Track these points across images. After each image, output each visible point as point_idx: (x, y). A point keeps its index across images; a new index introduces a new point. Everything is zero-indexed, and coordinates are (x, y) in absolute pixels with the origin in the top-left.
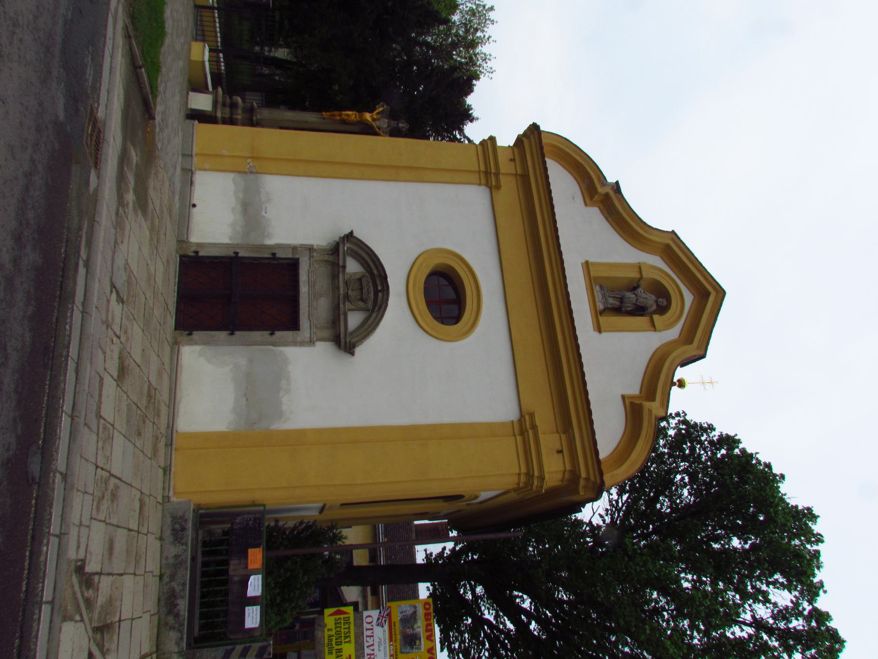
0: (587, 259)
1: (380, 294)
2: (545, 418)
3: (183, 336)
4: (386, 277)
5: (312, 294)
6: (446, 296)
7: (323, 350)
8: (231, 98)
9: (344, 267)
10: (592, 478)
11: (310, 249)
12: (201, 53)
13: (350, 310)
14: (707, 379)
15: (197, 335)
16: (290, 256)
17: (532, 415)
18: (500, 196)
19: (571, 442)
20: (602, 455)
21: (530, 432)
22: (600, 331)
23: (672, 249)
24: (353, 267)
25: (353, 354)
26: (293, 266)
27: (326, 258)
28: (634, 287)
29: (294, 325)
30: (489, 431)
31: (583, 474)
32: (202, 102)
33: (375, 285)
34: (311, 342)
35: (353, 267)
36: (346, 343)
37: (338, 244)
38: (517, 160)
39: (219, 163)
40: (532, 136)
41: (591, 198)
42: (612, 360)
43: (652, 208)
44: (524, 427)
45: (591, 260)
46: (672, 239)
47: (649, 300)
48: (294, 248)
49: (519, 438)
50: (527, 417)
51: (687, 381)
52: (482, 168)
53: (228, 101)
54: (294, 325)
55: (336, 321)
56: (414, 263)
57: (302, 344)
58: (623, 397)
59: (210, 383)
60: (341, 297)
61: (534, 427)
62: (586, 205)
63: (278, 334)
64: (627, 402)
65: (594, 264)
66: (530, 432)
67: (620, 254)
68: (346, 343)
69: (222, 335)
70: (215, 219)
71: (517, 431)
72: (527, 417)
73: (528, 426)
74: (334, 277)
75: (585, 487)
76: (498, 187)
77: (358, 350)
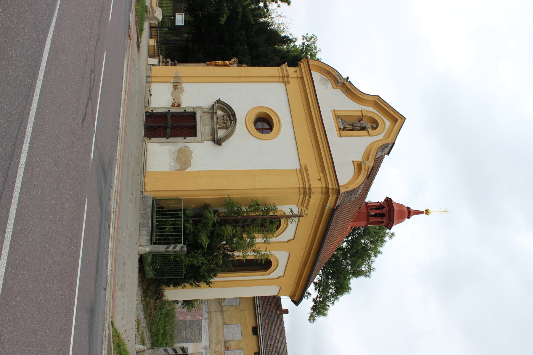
3: (146, 139)
4: (235, 114)
5: (202, 124)
6: (264, 123)
7: (209, 145)
8: (166, 60)
9: (216, 112)
10: (335, 188)
11: (201, 108)
12: (153, 42)
13: (219, 128)
15: (153, 139)
16: (192, 111)
17: (305, 166)
19: (325, 175)
23: (378, 103)
25: (220, 145)
28: (360, 119)
29: (195, 135)
30: (286, 172)
31: (331, 187)
32: (155, 61)
33: (230, 119)
34: (202, 141)
35: (220, 113)
36: (218, 142)
37: (213, 105)
39: (162, 80)
41: (336, 85)
42: (348, 150)
43: (365, 85)
44: (303, 171)
45: (336, 109)
46: (378, 99)
47: (368, 125)
53: (164, 61)
54: (195, 135)
55: (213, 133)
57: (198, 142)
58: (353, 162)
59: (161, 154)
62: (333, 88)
63: (187, 138)
64: (355, 164)
65: (337, 111)
66: (304, 172)
67: (351, 107)
68: (218, 142)
69: (164, 139)
70: (161, 99)
74: (212, 118)
75: (332, 193)
76: (289, 82)
77: (223, 144)
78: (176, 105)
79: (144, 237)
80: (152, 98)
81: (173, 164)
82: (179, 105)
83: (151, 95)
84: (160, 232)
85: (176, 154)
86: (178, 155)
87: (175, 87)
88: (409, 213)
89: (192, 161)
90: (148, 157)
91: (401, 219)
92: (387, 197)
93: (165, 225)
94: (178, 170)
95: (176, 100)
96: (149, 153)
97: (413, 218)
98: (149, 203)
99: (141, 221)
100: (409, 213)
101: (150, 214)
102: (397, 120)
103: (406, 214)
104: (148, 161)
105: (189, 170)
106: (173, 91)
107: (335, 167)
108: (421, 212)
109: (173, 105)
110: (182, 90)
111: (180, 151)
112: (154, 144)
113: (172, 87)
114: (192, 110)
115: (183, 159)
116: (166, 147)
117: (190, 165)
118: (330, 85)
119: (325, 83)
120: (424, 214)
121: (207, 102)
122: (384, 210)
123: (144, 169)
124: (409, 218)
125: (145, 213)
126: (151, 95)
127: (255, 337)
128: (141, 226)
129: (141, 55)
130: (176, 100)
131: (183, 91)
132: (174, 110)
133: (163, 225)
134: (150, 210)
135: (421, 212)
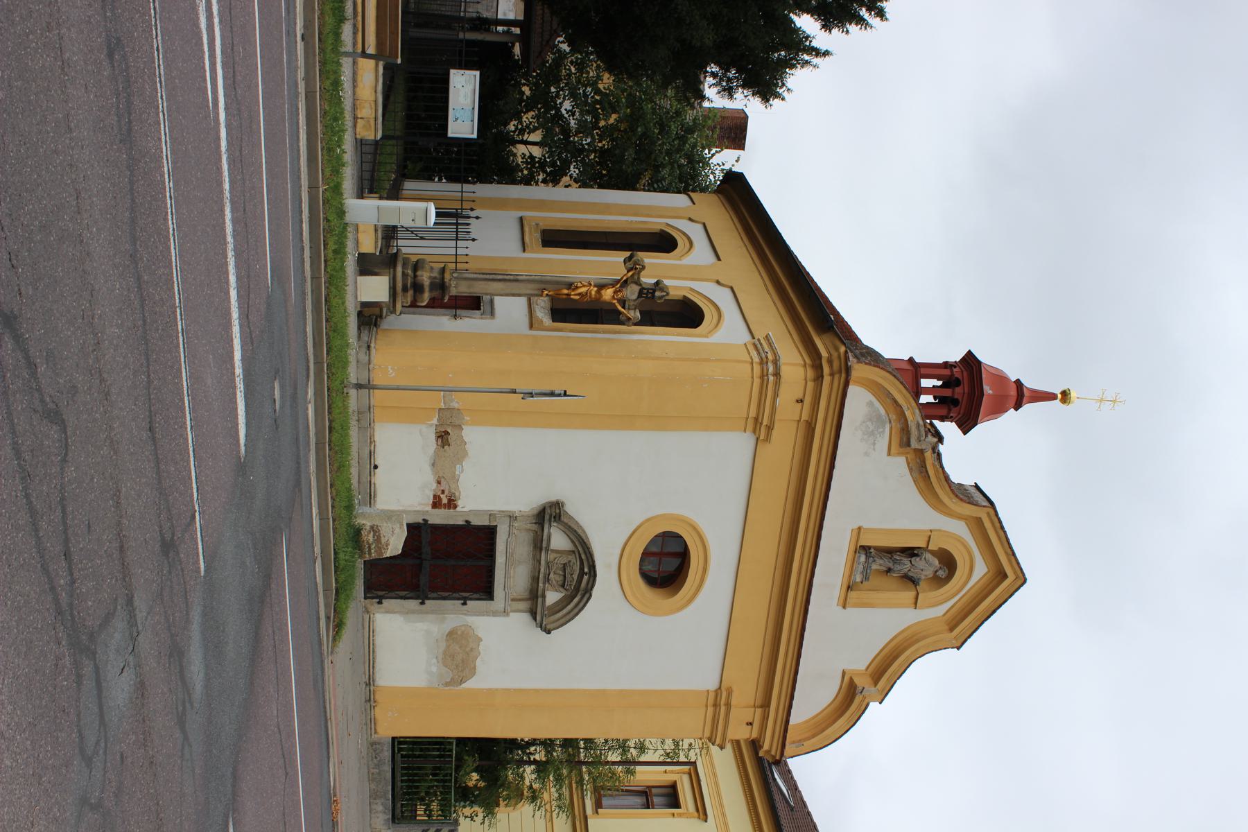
1: (586, 577)
3: (372, 604)
5: (511, 568)
7: (519, 621)
9: (544, 596)
11: (512, 517)
14: (1110, 395)
16: (487, 523)
17: (730, 692)
18: (764, 449)
19: (765, 718)
24: (558, 540)
26: (489, 533)
29: (485, 590)
34: (505, 613)
37: (544, 510)
38: (808, 400)
40: (837, 377)
48: (491, 515)
49: (711, 710)
51: (1073, 394)
52: (753, 414)
54: (485, 590)
55: (534, 597)
56: (634, 532)
59: (404, 643)
66: (723, 708)
69: (413, 604)
71: (711, 701)
72: (724, 694)
73: (723, 702)
78: (445, 501)
80: (380, 478)
81: (434, 669)
82: (452, 504)
83: (376, 467)
84: (409, 781)
85: (443, 645)
86: (448, 647)
87: (443, 437)
88: (1020, 396)
89: (478, 662)
90: (377, 650)
91: (998, 410)
93: (417, 787)
94: (447, 684)
95: (444, 486)
96: (379, 640)
97: (1027, 408)
98: (387, 754)
99: (373, 786)
100: (1020, 396)
101: (389, 775)
103: (1013, 401)
104: (378, 660)
105: (470, 684)
108: (1050, 397)
109: (436, 504)
110: (461, 455)
111: (451, 634)
114: (484, 521)
115: (459, 656)
116: (420, 625)
117: (473, 672)
118: (883, 442)
119: (872, 433)
120: (1058, 401)
121: (525, 502)
122: (958, 390)
124: (1016, 409)
125: (379, 774)
126: (376, 467)
128: (374, 796)
129: (337, 649)
130: (444, 486)
131: (465, 454)
132: (440, 517)
133: (416, 775)
134: (387, 769)
135: (1050, 397)
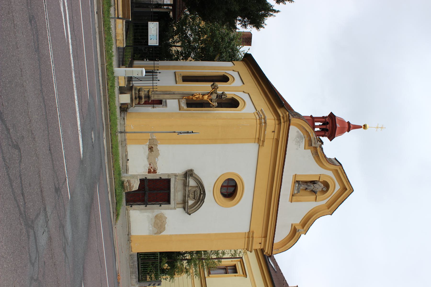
0: (296, 173)
1: (202, 195)
2: (258, 232)
5: (176, 192)
7: (180, 211)
11: (176, 175)
16: (167, 178)
17: (253, 233)
18: (263, 149)
19: (265, 241)
20: (275, 242)
21: (251, 238)
22: (291, 202)
24: (192, 183)
27: (182, 178)
29: (168, 201)
34: (175, 208)
40: (286, 123)
49: (247, 239)
50: (251, 233)
51: (368, 126)
52: (257, 137)
54: (168, 201)
56: (218, 179)
57: (171, 209)
60: (187, 195)
61: (253, 237)
66: (251, 238)
69: (143, 207)
71: (247, 236)
72: (251, 233)
76: (263, 145)
78: (152, 171)
79: (134, 280)
80: (130, 164)
81: (151, 229)
82: (155, 172)
83: (128, 160)
85: (154, 220)
86: (155, 221)
88: (349, 127)
89: (166, 226)
92: (331, 141)
93: (147, 269)
94: (155, 234)
95: (152, 166)
96: (132, 219)
97: (352, 131)
98: (136, 259)
99: (131, 270)
100: (349, 127)
102: (346, 189)
103: (347, 129)
105: (163, 233)
106: (149, 154)
107: (287, 153)
108: (360, 127)
109: (149, 172)
110: (157, 155)
111: (156, 217)
112: (135, 211)
113: (147, 149)
115: (159, 224)
117: (164, 229)
118: (303, 145)
119: (299, 142)
121: (180, 170)
123: (129, 234)
126: (128, 160)
127: (184, 178)
128: (132, 273)
130: (152, 166)
131: (159, 154)
132: (151, 176)
134: (136, 263)
135: (360, 127)
